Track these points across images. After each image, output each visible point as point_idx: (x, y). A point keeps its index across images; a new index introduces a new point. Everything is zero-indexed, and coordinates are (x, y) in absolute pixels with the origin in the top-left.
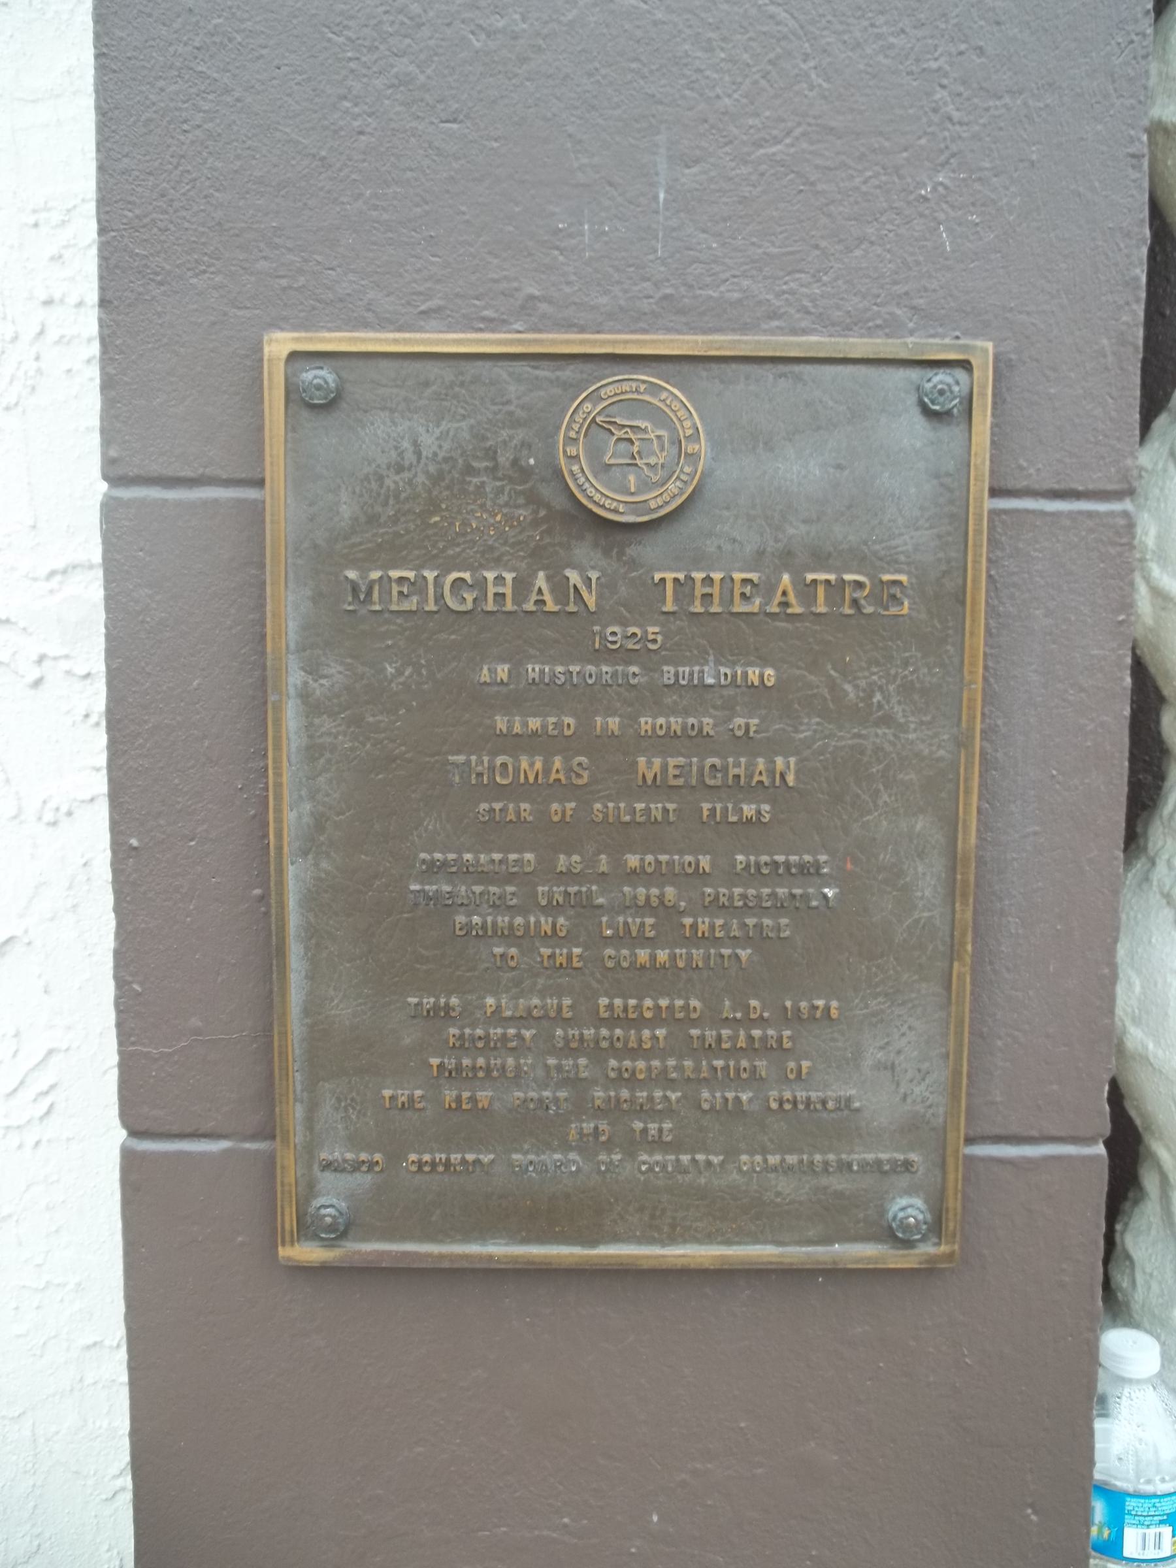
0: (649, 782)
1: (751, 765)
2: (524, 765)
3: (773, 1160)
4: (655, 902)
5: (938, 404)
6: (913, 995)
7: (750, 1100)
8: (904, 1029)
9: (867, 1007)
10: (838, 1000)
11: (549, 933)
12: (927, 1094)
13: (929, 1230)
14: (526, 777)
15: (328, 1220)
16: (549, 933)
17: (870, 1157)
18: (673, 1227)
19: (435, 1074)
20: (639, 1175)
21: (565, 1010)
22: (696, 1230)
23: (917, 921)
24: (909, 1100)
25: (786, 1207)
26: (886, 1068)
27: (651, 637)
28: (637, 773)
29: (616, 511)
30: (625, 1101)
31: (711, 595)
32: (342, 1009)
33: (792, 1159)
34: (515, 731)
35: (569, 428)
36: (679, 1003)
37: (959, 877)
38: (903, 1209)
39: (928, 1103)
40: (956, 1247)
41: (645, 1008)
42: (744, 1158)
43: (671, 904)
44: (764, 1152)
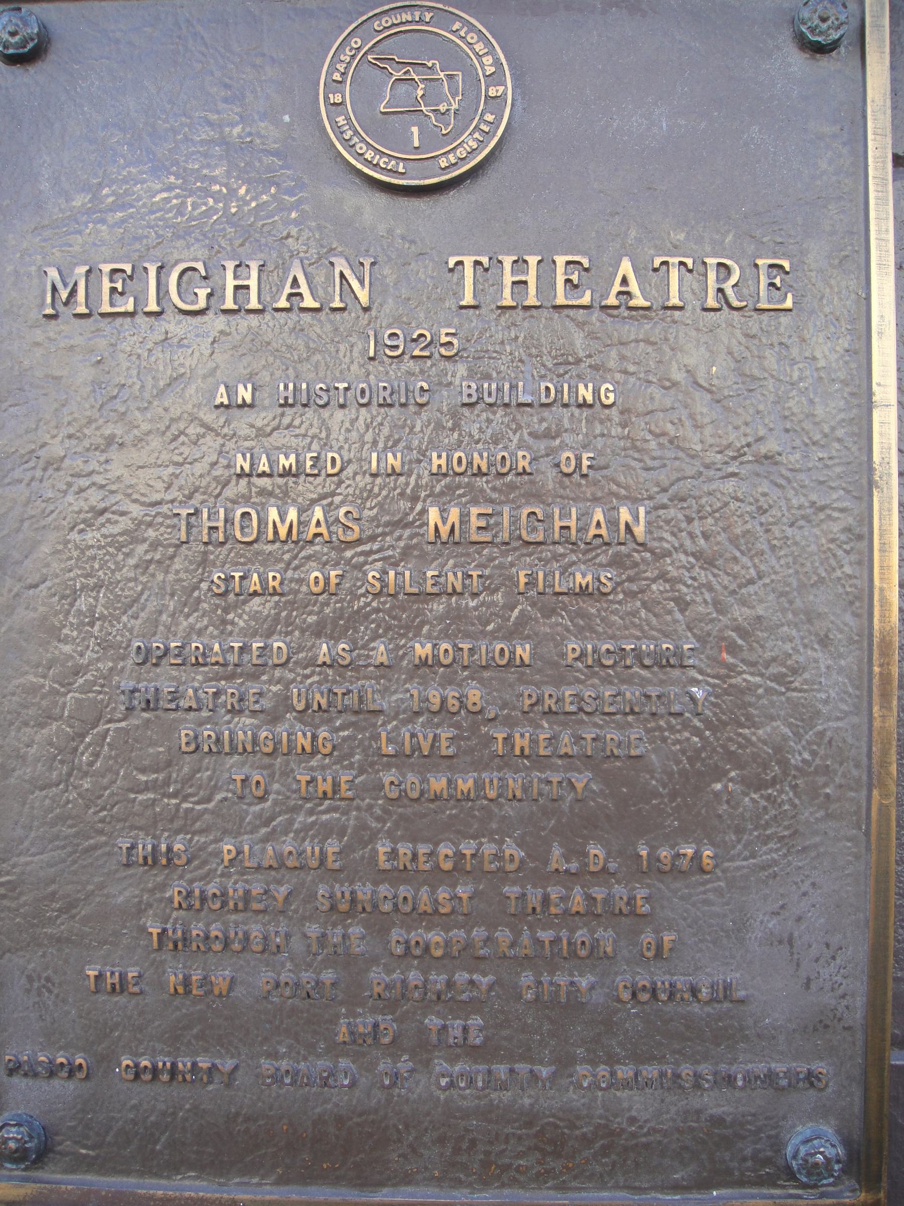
0: (444, 536)
1: (584, 516)
2: (273, 514)
3: (625, 1072)
4: (453, 704)
5: (821, 33)
6: (817, 839)
7: (592, 988)
8: (806, 886)
9: (753, 855)
10: (713, 844)
11: (308, 749)
12: (839, 978)
13: (842, 1170)
14: (276, 532)
15: (12, 1145)
16: (308, 749)
17: (760, 1068)
18: (486, 1164)
19: (155, 945)
20: (439, 1092)
21: (331, 858)
22: (517, 1170)
23: (821, 734)
24: (813, 986)
25: (643, 1140)
26: (780, 942)
27: (444, 339)
28: (427, 524)
29: (393, 172)
30: (416, 987)
31: (525, 283)
32: (34, 855)
33: (651, 1071)
34: (261, 469)
35: (332, 68)
36: (489, 849)
37: (876, 669)
38: (807, 1141)
39: (841, 991)
40: (882, 1195)
41: (441, 857)
42: (582, 1069)
43: (476, 709)
44: (612, 1060)
